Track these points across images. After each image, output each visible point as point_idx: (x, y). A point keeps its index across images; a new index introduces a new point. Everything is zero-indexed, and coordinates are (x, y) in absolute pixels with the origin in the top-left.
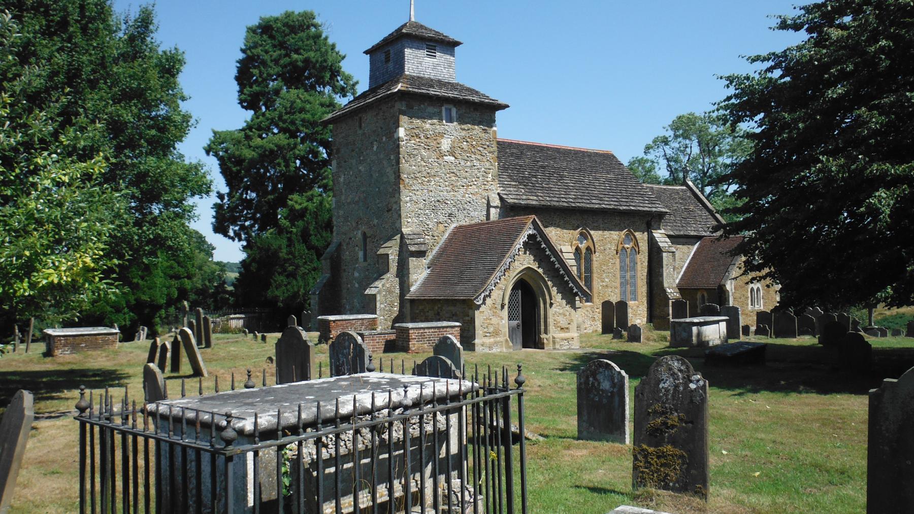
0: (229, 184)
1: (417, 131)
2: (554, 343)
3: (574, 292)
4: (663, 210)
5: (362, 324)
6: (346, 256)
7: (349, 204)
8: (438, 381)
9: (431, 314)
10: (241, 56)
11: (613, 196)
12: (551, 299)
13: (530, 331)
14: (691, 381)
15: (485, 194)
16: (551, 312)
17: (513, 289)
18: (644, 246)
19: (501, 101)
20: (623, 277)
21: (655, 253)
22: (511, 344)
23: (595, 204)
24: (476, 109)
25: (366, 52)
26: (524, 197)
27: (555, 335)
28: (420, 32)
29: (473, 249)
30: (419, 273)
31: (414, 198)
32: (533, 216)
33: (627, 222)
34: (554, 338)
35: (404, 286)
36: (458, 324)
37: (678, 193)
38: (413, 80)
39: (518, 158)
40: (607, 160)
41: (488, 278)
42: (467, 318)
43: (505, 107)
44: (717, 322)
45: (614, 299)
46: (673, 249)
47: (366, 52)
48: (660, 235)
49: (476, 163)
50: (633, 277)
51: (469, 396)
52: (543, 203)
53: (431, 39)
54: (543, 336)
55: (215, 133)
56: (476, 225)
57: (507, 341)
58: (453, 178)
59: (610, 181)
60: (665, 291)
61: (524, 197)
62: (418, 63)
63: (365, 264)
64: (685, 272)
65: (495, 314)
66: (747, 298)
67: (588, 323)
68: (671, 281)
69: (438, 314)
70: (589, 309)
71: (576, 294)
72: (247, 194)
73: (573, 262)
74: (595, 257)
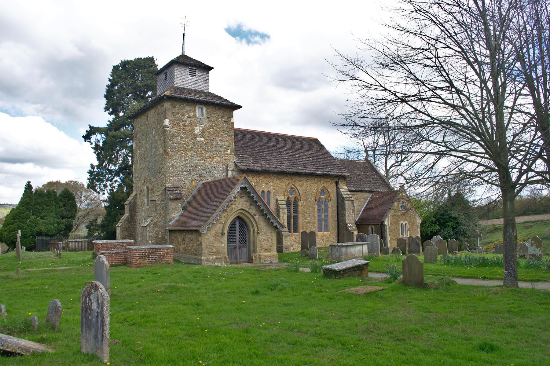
0: (98, 158)
1: (178, 122)
2: (260, 259)
4: (346, 174)
6: (139, 202)
7: (141, 169)
10: (109, 83)
11: (314, 165)
12: (258, 230)
18: (334, 197)
19: (237, 103)
20: (319, 216)
23: (301, 170)
24: (219, 109)
26: (252, 165)
27: (261, 254)
31: (175, 164)
32: (245, 175)
33: (323, 181)
34: (260, 255)
35: (166, 221)
36: (171, 246)
37: (361, 165)
39: (253, 140)
41: (211, 216)
42: (198, 242)
43: (240, 107)
44: (362, 245)
48: (344, 189)
50: (326, 216)
52: (264, 168)
55: (90, 127)
58: (203, 152)
59: (313, 156)
60: (346, 225)
61: (252, 165)
63: (148, 207)
65: (217, 240)
66: (399, 230)
70: (296, 237)
72: (109, 166)
73: (285, 206)
74: (300, 203)
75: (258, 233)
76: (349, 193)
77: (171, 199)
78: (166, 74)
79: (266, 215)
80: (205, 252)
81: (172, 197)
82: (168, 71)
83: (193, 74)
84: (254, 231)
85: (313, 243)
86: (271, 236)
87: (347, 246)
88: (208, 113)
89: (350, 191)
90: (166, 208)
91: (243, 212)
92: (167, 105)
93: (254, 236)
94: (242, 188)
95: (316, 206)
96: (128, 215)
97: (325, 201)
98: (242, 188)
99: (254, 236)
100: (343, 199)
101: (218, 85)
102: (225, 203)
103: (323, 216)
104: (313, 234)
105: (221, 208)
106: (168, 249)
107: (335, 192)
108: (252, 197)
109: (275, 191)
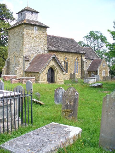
3: (64, 70)
5: (13, 77)
6: (11, 60)
8: (12, 92)
9: (30, 75)
13: (51, 80)
14: (75, 93)
15: (43, 47)
16: (57, 75)
17: (48, 71)
18: (80, 61)
19: (48, 26)
20: (75, 68)
21: (82, 62)
22: (48, 82)
23: (69, 51)
25: (17, 13)
26: (53, 48)
28: (29, 9)
29: (40, 59)
30: (27, 66)
32: (54, 53)
35: (24, 68)
36: (34, 78)
38: (27, 20)
40: (73, 41)
42: (38, 76)
45: (73, 73)
46: (87, 62)
47: (17, 13)
48: (84, 58)
49: (42, 40)
50: (77, 68)
51: (20, 96)
52: (57, 50)
53: (32, 11)
54: (56, 81)
56: (41, 54)
57: (47, 82)
62: (28, 16)
64: (89, 67)
67: (67, 78)
68: (86, 69)
69: (31, 75)
71: (63, 71)
73: (64, 64)
74: (69, 63)
75: (58, 73)
76: (85, 59)
77: (25, 61)
78: (22, 14)
79: (60, 67)
80: (40, 79)
81: (26, 60)
82: (23, 13)
83: (32, 14)
84: (56, 73)
85: (74, 78)
86: (61, 75)
87: (90, 79)
88: (38, 29)
89: (86, 59)
90: (24, 64)
91: (53, 66)
92: (24, 26)
93: (56, 74)
94: (53, 58)
95: (74, 64)
96: (6, 66)
97: (77, 62)
98: (53, 58)
99: (56, 74)
100: (83, 62)
101: (40, 19)
102: (47, 63)
103: (76, 68)
104: (74, 74)
105: (46, 64)
106: (33, 78)
107: (81, 59)
108: (56, 61)
109: (61, 58)
